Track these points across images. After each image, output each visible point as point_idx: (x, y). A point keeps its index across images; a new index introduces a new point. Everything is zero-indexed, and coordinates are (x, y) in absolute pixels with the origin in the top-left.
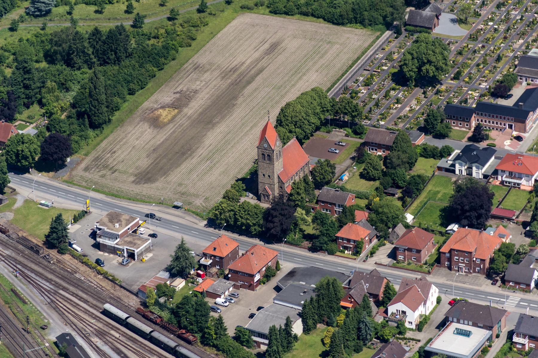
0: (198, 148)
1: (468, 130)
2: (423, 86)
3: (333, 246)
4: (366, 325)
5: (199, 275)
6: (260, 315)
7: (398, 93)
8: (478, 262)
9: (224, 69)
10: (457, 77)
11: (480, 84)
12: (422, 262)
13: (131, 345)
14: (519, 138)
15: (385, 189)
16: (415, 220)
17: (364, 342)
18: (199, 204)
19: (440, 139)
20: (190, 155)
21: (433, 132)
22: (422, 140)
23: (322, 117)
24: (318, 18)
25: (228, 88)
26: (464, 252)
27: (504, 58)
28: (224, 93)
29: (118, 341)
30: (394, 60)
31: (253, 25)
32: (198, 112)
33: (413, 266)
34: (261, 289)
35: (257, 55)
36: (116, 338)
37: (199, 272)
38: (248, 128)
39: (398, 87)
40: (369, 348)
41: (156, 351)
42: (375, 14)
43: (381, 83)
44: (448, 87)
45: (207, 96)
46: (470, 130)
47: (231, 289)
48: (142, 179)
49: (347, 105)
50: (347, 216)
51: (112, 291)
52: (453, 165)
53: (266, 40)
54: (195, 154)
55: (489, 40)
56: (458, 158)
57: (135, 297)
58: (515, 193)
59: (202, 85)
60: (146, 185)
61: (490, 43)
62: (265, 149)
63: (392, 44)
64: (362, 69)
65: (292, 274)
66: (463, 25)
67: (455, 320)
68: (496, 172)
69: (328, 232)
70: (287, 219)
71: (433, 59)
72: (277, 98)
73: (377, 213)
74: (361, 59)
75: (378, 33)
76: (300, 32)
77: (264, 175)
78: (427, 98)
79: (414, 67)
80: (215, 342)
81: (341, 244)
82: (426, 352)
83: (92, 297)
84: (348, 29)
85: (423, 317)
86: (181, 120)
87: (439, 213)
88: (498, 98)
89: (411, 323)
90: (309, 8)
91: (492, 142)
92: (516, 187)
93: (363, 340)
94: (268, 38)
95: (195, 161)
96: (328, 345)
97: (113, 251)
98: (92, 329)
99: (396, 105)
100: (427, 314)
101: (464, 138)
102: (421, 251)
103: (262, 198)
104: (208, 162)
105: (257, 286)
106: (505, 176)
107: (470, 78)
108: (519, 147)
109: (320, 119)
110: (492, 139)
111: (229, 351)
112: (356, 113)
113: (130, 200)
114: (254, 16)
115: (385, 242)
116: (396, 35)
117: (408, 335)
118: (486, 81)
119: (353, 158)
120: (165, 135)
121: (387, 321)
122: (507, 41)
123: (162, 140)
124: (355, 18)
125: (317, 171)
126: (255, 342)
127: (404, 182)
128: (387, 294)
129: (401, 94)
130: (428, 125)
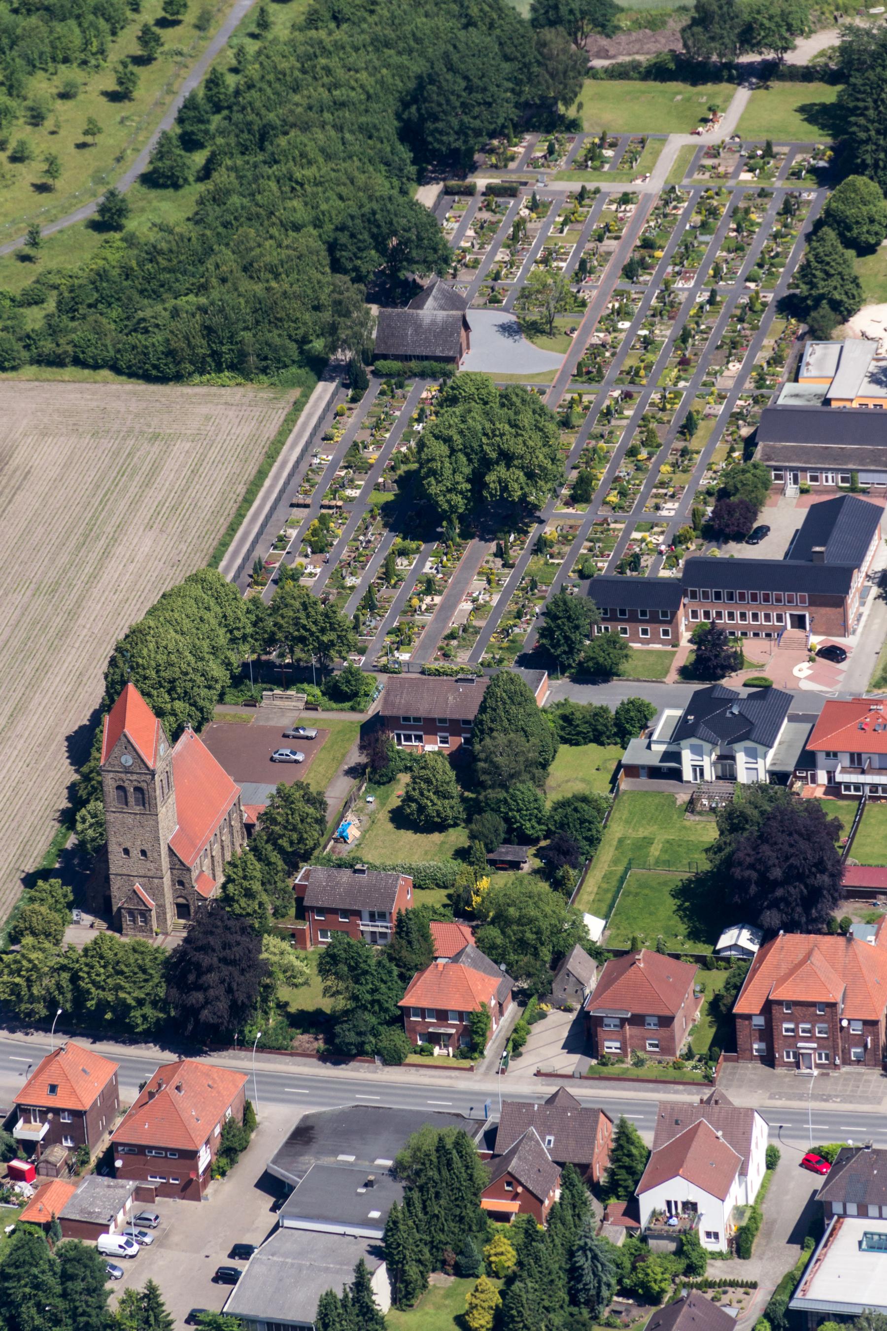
1: (669, 648)
2: (486, 534)
3: (395, 1037)
4: (595, 1257)
5: (16, 1175)
6: (259, 1269)
7: (422, 563)
8: (856, 1029)
10: (581, 494)
11: (657, 508)
12: (678, 1053)
14: (834, 654)
15: (490, 851)
16: (607, 933)
17: (592, 1310)
19: (594, 683)
21: (570, 666)
22: (548, 692)
23: (234, 659)
24: (96, 367)
26: (813, 1004)
27: (701, 424)
30: (371, 466)
33: (651, 1068)
34: (217, 1192)
37: (15, 1163)
39: (414, 545)
40: (608, 1325)
42: (275, 337)
43: (356, 539)
44: (566, 528)
46: (675, 645)
47: (129, 1204)
49: (302, 615)
50: (409, 948)
52: (675, 756)
55: (637, 374)
58: (881, 817)
61: (644, 382)
63: (350, 420)
64: (284, 503)
65: (303, 1136)
66: (543, 339)
67: (852, 1209)
68: (807, 761)
70: (243, 972)
71: (515, 446)
72: (58, 621)
73: (501, 920)
74: (271, 474)
75: (296, 393)
76: (55, 417)
77: (126, 851)
78: (512, 566)
79: (459, 478)
82: (792, 1314)
85: (748, 1214)
87: (671, 904)
88: (726, 542)
89: (717, 1236)
90: (61, 341)
91: (756, 674)
92: (880, 798)
93: (587, 1303)
99: (428, 600)
100: (751, 1202)
101: (667, 672)
102: (673, 1018)
103: (127, 920)
105: (205, 1184)
106: (839, 768)
107: (623, 494)
108: (841, 678)
109: (228, 665)
110: (752, 666)
112: (331, 636)
115: (543, 1006)
116: (350, 392)
117: (714, 1271)
118: (673, 496)
119: (355, 772)
121: (644, 1239)
122: (692, 371)
124: (215, 355)
125: (279, 819)
127: (539, 822)
128: (626, 1159)
129: (428, 564)
130: (556, 646)
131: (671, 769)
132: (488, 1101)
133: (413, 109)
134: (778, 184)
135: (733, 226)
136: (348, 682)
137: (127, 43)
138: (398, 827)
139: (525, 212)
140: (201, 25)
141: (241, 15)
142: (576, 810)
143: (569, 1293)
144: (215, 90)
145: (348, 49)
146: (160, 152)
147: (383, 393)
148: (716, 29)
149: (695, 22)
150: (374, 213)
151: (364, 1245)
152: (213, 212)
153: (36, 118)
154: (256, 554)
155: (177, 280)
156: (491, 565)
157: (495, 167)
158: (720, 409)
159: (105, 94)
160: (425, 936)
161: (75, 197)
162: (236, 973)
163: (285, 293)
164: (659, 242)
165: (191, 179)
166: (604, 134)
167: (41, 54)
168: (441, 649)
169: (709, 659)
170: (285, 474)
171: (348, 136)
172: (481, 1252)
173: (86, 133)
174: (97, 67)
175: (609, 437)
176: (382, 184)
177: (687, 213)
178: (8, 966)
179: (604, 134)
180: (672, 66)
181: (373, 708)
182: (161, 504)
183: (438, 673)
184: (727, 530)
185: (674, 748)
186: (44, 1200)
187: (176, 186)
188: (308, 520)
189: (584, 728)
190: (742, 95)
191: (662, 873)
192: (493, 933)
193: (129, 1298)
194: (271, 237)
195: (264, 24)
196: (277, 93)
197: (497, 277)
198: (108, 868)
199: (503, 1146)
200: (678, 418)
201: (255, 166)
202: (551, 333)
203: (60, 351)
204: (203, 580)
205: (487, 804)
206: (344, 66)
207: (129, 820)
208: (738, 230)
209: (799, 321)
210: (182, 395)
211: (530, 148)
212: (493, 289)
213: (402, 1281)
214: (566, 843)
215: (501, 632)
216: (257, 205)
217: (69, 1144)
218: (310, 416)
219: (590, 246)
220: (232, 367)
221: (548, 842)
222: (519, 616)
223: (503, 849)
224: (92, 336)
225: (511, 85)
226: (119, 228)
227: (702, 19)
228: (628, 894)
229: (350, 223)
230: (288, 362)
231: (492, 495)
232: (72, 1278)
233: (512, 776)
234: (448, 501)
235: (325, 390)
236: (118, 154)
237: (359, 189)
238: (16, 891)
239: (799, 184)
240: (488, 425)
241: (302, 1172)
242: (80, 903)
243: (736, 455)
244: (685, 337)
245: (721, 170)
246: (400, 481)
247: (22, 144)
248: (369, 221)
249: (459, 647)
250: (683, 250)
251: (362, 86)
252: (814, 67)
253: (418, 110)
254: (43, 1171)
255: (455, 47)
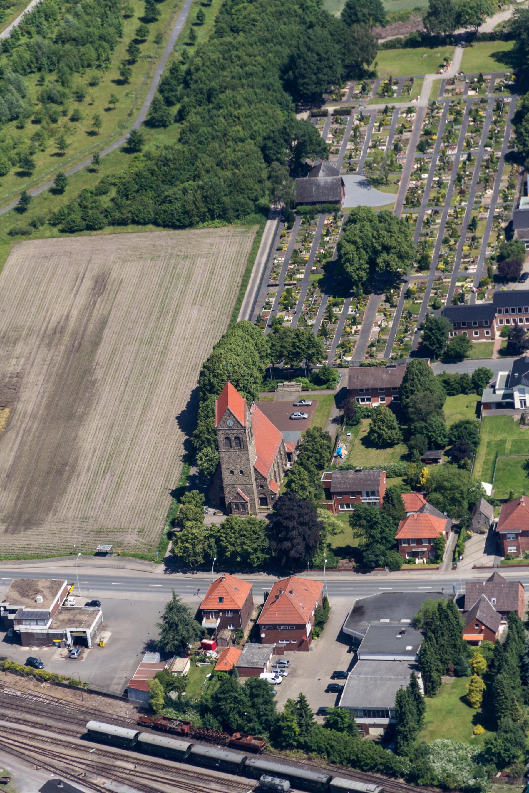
0: (77, 458)
1: (490, 341)
2: (378, 291)
5: (207, 647)
6: (352, 682)
7: (346, 309)
9: (42, 332)
10: (423, 265)
11: (466, 269)
13: (162, 776)
15: (422, 454)
18: (133, 542)
20: (72, 472)
21: (440, 355)
22: (436, 368)
23: (263, 367)
24: (145, 224)
25: (68, 359)
28: (65, 368)
29: (137, 774)
30: (307, 261)
31: (46, 257)
32: (43, 405)
35: (81, 300)
36: (130, 770)
37: (205, 641)
38: (139, 412)
39: (340, 300)
41: (208, 776)
42: (241, 198)
45: (41, 378)
46: (493, 338)
47: (271, 657)
48: (17, 524)
49: (296, 341)
51: (79, 702)
52: (511, 396)
53: (81, 275)
54: (78, 469)
55: (438, 200)
56: (511, 382)
57: (122, 703)
59: (21, 363)
60: (29, 532)
61: (443, 204)
62: (230, 429)
63: (290, 239)
64: (264, 285)
65: (358, 611)
66: (383, 187)
69: (384, 535)
70: (310, 528)
72: (156, 358)
73: (440, 488)
74: (254, 270)
75: (256, 227)
77: (232, 472)
78: (396, 306)
79: (363, 262)
80: (302, 740)
81: (407, 550)
83: (53, 718)
84: (202, 231)
86: (22, 422)
88: (507, 283)
90: (124, 211)
94: (83, 270)
95: (84, 478)
96: (479, 705)
97: (47, 640)
98: (83, 767)
99: (354, 328)
103: (234, 508)
104: (108, 476)
107: (446, 263)
109: (260, 370)
111: (332, 747)
113: (18, 559)
114: (38, 242)
116: (286, 224)
120: (11, 450)
122: (468, 196)
123: (11, 459)
125: (309, 448)
126: (361, 726)
127: (445, 437)
131: (507, 403)
132: (454, 584)
133: (291, 73)
134: (489, 95)
135: (471, 119)
136: (324, 374)
137: (120, 53)
138: (367, 447)
139: (357, 122)
140: (158, 41)
141: (178, 34)
142: (466, 428)
143: (521, 679)
144: (176, 74)
145: (247, 46)
146: (155, 108)
147: (303, 223)
148: (442, 17)
149: (430, 15)
150: (285, 128)
151: (406, 665)
152: (192, 137)
153: (80, 97)
154: (257, 312)
155: (181, 174)
156: (384, 307)
157: (335, 100)
158: (487, 215)
159: (114, 81)
160: (400, 501)
161: (111, 136)
162: (307, 530)
163: (243, 175)
164: (434, 131)
165: (172, 121)
166: (391, 78)
167: (76, 64)
168: (367, 353)
169: (516, 344)
170: (261, 270)
171: (258, 91)
172: (467, 662)
173: (110, 102)
174: (106, 68)
175: (431, 234)
176: (281, 115)
177: (444, 115)
178: (180, 538)
179: (391, 78)
180: (419, 39)
181: (338, 388)
182: (197, 292)
183: (369, 365)
184: (508, 277)
185: (509, 392)
186: (227, 658)
187: (165, 126)
188: (279, 292)
189: (456, 386)
190: (459, 51)
191: (514, 457)
192: (437, 495)
193: (290, 704)
194: (229, 147)
195: (193, 37)
196: (213, 72)
197: (350, 157)
198: (222, 482)
199: (469, 606)
200: (465, 222)
201: (209, 111)
202: (387, 184)
203: (124, 217)
204: (243, 327)
205: (416, 430)
206: (247, 54)
207: (233, 455)
208: (474, 121)
209: (518, 165)
210: (195, 234)
211: (351, 89)
212: (350, 164)
213: (430, 682)
214: (461, 446)
215: (399, 340)
216: (216, 131)
217: (232, 628)
218: (267, 239)
219: (396, 136)
220: (220, 217)
221: (450, 447)
222: (406, 331)
223: (428, 453)
224: (141, 207)
225: (340, 56)
226: (139, 150)
227: (433, 12)
228: (499, 470)
229: (272, 135)
230: (249, 211)
231: (381, 270)
232: (257, 696)
233: (428, 414)
234: (358, 275)
235: (272, 225)
236: (129, 112)
237: (270, 118)
238: (169, 501)
239: (501, 94)
240: (375, 233)
241: (361, 630)
242: (208, 503)
243: (501, 237)
244: (460, 179)
245: (457, 91)
246: (324, 267)
247: (77, 111)
248: (282, 133)
249: (377, 351)
250: (447, 134)
251: (259, 64)
252: (495, 33)
253: (294, 73)
254: (219, 644)
255: (309, 38)
